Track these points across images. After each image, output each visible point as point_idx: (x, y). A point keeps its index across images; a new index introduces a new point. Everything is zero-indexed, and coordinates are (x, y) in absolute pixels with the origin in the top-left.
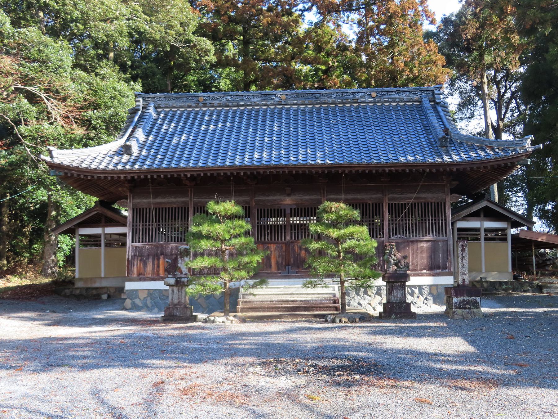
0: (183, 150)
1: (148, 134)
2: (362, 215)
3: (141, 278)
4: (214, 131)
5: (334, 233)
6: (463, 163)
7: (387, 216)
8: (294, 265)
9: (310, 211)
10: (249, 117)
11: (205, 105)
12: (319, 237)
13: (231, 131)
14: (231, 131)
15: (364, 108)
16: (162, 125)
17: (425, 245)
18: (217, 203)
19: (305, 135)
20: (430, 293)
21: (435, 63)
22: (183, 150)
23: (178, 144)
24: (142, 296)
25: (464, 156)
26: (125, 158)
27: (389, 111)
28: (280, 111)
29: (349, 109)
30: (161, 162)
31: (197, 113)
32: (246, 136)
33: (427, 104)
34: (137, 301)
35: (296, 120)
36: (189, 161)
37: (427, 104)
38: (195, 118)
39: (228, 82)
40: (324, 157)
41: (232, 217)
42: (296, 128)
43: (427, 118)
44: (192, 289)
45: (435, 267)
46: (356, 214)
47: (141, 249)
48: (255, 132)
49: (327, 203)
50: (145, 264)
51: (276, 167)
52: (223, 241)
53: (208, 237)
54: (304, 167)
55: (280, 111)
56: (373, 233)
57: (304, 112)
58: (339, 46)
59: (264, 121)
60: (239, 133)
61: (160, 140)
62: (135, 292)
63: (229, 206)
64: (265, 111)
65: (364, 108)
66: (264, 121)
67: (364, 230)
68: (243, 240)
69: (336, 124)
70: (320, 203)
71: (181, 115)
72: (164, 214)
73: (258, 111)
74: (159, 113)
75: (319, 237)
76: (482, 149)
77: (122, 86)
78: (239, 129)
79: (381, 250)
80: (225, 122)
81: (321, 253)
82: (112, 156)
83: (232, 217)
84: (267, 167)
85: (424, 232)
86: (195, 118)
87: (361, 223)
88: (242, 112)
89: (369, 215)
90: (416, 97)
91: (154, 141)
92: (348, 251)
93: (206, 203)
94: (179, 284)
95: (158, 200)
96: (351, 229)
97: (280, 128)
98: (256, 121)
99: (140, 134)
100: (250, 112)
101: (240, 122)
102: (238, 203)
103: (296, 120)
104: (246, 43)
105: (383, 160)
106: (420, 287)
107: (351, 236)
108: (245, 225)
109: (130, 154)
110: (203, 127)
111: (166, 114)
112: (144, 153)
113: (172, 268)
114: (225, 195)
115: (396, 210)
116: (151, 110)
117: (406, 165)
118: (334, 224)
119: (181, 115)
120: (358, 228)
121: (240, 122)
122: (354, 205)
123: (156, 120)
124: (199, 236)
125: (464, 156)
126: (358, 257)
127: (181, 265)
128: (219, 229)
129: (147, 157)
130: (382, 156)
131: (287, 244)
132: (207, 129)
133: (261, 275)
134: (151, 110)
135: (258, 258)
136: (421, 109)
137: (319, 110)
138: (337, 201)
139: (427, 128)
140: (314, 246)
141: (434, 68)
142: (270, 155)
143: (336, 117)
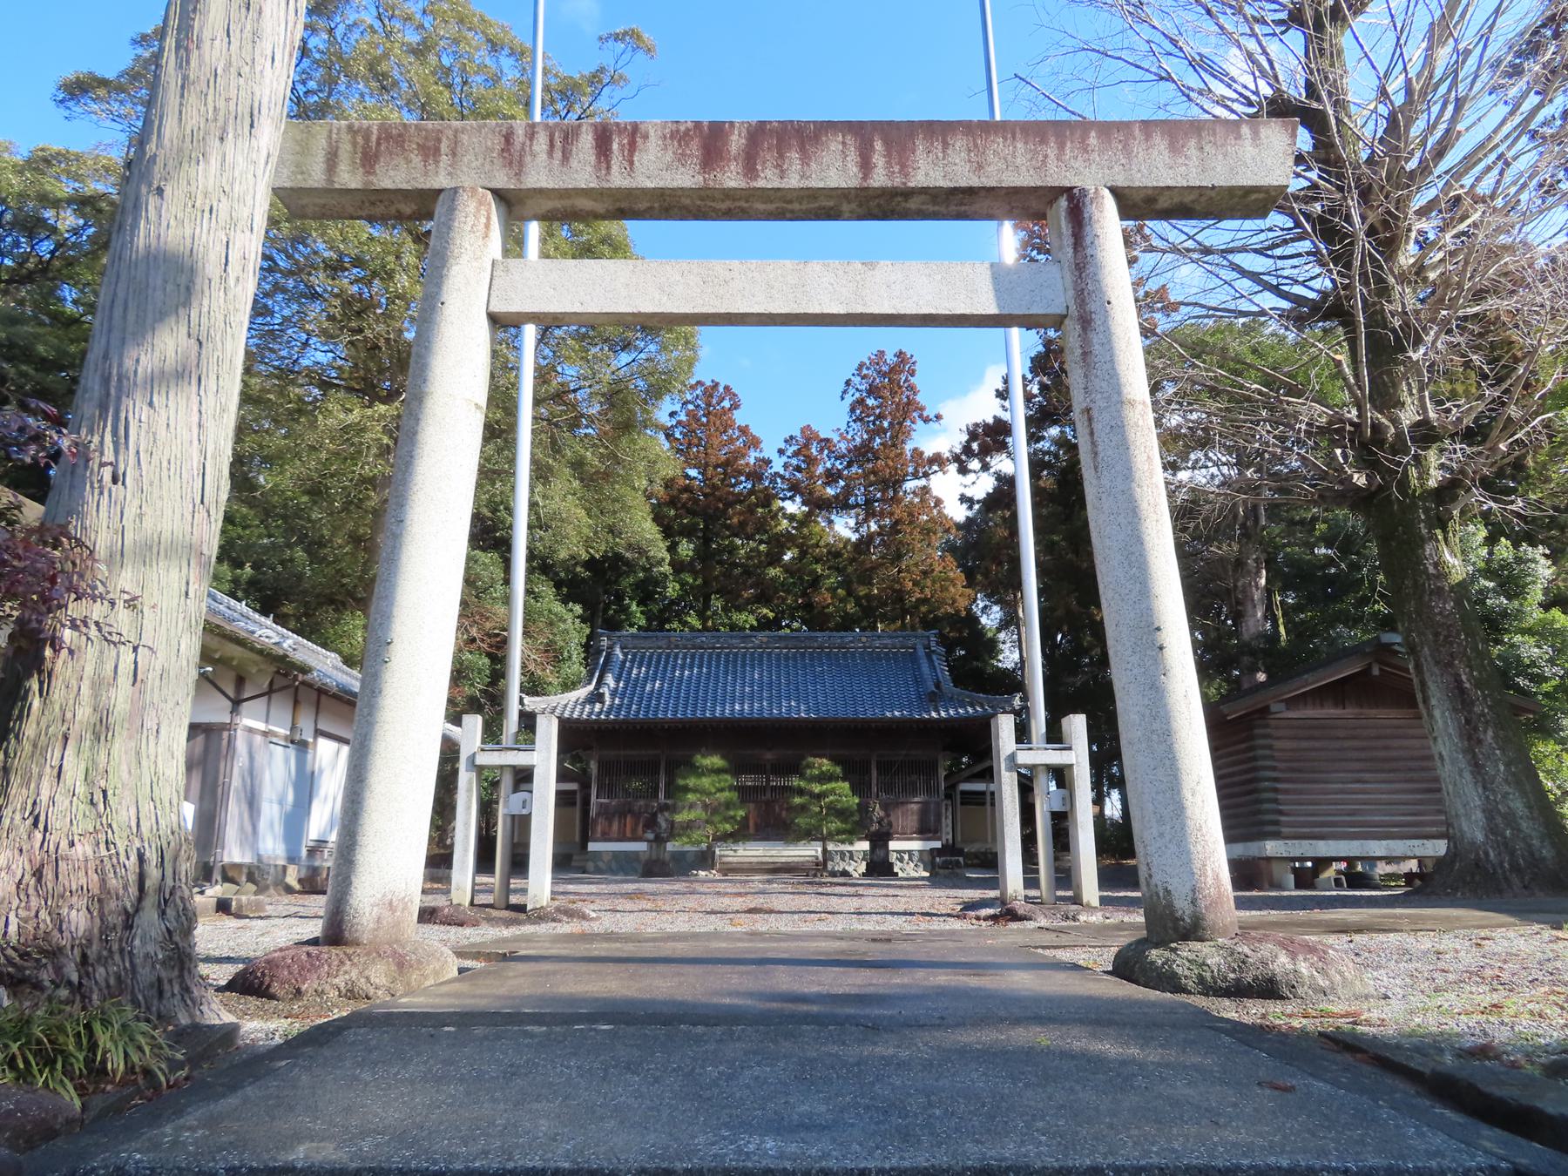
0: (659, 699)
1: (618, 681)
2: (844, 770)
3: (606, 838)
4: (690, 677)
5: (817, 788)
6: (949, 720)
7: (874, 773)
8: (774, 826)
9: (795, 768)
10: (727, 661)
11: (677, 647)
12: (801, 792)
13: (708, 679)
14: (708, 679)
15: (853, 654)
16: (631, 669)
17: (915, 807)
18: (704, 756)
19: (788, 684)
20: (921, 860)
21: (953, 582)
22: (659, 699)
23: (652, 691)
24: (606, 858)
25: (952, 712)
26: (598, 706)
27: (880, 659)
28: (761, 655)
29: (836, 654)
30: (635, 712)
31: (668, 656)
32: (725, 685)
33: (921, 652)
34: (600, 864)
35: (778, 666)
36: (667, 712)
37: (921, 652)
38: (667, 662)
39: (678, 587)
40: (808, 711)
41: (719, 771)
42: (779, 676)
43: (919, 668)
44: (671, 846)
45: (925, 831)
46: (838, 770)
47: (607, 805)
48: (735, 680)
49: (811, 759)
50: (610, 825)
51: (758, 720)
52: (709, 794)
53: (695, 791)
54: (788, 720)
55: (761, 655)
56: (855, 790)
57: (787, 658)
58: (829, 552)
59: (744, 666)
60: (717, 681)
61: (631, 688)
62: (597, 854)
63: (715, 761)
64: (744, 655)
65: (853, 654)
66: (744, 666)
67: (847, 785)
68: (727, 794)
69: (823, 672)
70: (803, 758)
71: (651, 658)
72: (633, 769)
73: (736, 655)
74: (625, 655)
75: (801, 792)
76: (972, 706)
77: (558, 608)
78: (717, 676)
79: (863, 808)
80: (700, 667)
81: (803, 808)
82: (583, 704)
83: (719, 771)
84: (750, 720)
85: (914, 792)
86: (667, 662)
87: (844, 780)
88: (719, 656)
89: (855, 773)
90: (910, 643)
91: (625, 689)
92: (830, 807)
93: (691, 756)
94: (659, 840)
95: (629, 752)
96: (833, 785)
97: (761, 676)
98: (735, 666)
99: (610, 680)
100: (727, 655)
101: (718, 666)
102: (723, 757)
103: (778, 666)
104: (707, 541)
105: (869, 714)
106: (910, 852)
107: (833, 791)
108: (728, 779)
109: (603, 703)
110: (677, 673)
111: (634, 655)
112: (617, 701)
113: (651, 823)
114: (713, 749)
115: (884, 768)
116: (618, 651)
117: (893, 720)
118: (813, 779)
119: (651, 658)
120: (840, 784)
121: (718, 666)
122: (835, 760)
123: (624, 662)
124: (686, 789)
125: (943, 714)
126: (842, 814)
127: (661, 820)
128: (706, 782)
129: (620, 706)
130: (869, 711)
131: (767, 803)
132: (682, 675)
133: (741, 834)
134: (618, 651)
135: (741, 813)
136: (913, 658)
137: (803, 655)
138: (821, 756)
139: (918, 680)
140: (797, 800)
141: (952, 589)
142: (752, 707)
143: (821, 665)
